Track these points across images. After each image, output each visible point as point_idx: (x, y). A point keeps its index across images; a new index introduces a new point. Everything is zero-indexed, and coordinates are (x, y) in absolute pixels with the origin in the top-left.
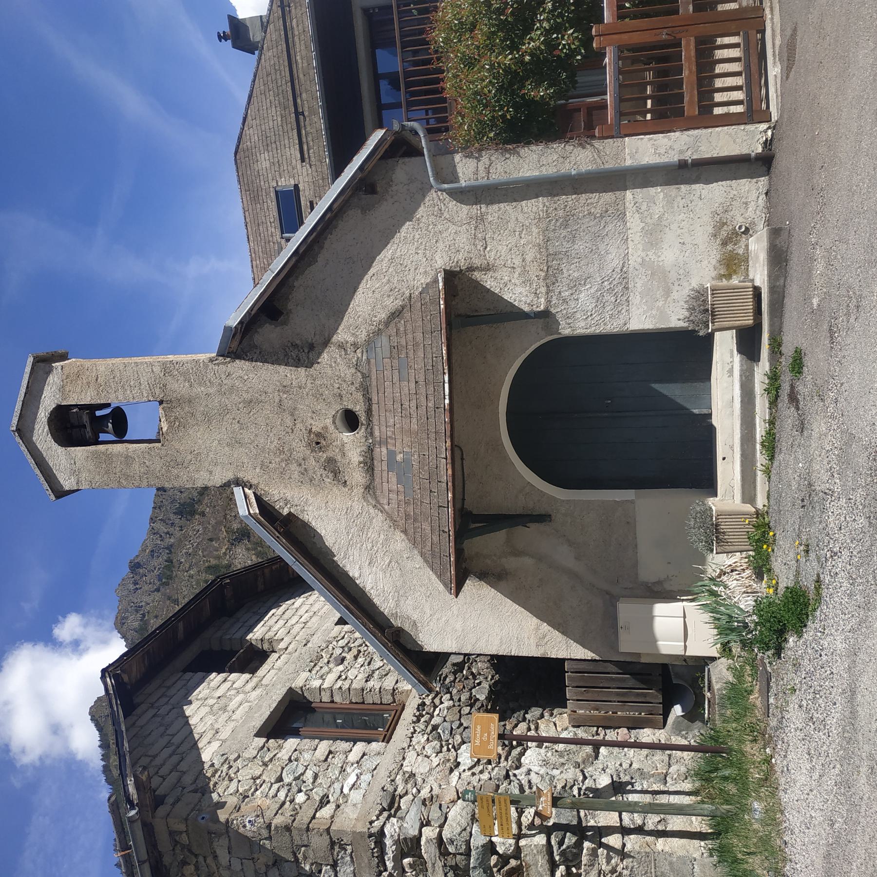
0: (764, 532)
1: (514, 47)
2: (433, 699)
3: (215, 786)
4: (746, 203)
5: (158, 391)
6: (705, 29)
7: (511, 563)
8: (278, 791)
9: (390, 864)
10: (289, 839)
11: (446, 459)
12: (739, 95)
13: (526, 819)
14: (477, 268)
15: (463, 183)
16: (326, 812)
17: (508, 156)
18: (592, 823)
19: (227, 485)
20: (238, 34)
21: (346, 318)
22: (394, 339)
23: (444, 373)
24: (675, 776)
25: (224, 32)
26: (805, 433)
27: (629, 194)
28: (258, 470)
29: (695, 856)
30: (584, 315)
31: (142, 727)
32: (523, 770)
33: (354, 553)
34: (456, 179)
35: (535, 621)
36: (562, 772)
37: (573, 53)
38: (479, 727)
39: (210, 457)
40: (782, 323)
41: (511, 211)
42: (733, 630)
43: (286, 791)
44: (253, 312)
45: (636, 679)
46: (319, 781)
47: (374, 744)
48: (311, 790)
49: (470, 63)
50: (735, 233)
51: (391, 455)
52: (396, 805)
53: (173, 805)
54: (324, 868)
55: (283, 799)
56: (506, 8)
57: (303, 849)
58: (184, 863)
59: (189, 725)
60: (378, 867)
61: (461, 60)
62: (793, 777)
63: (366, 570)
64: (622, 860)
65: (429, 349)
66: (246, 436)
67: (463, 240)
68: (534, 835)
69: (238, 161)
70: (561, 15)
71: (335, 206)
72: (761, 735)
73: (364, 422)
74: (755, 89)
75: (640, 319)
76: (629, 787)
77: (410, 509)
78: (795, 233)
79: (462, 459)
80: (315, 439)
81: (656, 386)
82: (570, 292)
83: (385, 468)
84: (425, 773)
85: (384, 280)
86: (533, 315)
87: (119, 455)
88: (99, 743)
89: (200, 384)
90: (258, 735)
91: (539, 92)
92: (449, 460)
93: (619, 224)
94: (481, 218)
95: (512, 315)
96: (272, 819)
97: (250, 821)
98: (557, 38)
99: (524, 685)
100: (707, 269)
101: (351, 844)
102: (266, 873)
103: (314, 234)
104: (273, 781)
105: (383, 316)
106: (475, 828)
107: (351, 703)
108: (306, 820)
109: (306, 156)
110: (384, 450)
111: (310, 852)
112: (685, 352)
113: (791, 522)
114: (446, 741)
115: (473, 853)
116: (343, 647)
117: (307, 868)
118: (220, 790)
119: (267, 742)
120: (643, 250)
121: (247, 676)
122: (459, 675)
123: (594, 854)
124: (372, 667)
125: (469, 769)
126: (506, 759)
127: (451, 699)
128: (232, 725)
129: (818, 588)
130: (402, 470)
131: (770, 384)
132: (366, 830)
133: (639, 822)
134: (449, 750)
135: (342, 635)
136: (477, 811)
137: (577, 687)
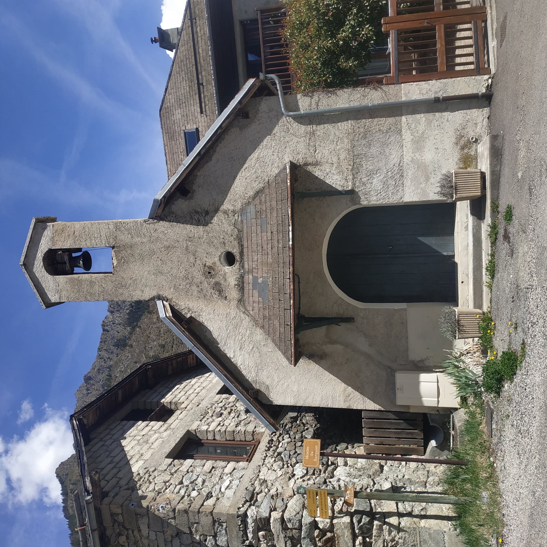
0: (488, 323)
1: (333, 36)
2: (278, 437)
3: (140, 486)
4: (476, 124)
5: (111, 240)
6: (450, 20)
7: (329, 348)
8: (180, 489)
9: (250, 536)
10: (186, 519)
11: (290, 279)
12: (471, 59)
13: (337, 508)
14: (310, 164)
15: (302, 112)
16: (210, 502)
17: (330, 95)
18: (379, 510)
19: (153, 299)
20: (164, 39)
21: (229, 195)
22: (258, 207)
23: (289, 225)
24: (432, 483)
25: (155, 38)
26: (514, 256)
27: (404, 118)
28: (172, 290)
29: (445, 530)
30: (376, 193)
31: (94, 452)
32: (335, 479)
33: (231, 342)
34: (298, 109)
35: (343, 385)
36: (360, 480)
37: (369, 39)
38: (308, 448)
39: (143, 282)
40: (499, 193)
41: (331, 129)
42: (469, 385)
43: (185, 490)
44: (172, 191)
45: (407, 423)
46: (206, 484)
47: (241, 463)
48: (201, 489)
49: (306, 47)
50: (469, 142)
51: (255, 279)
52: (255, 499)
53: (114, 497)
54: (208, 538)
55: (183, 494)
56: (328, 12)
57: (195, 525)
58: (120, 534)
59: (124, 451)
60: (243, 537)
61: (300, 46)
62: (508, 471)
63: (238, 353)
64: (398, 533)
65: (280, 211)
66: (166, 269)
67: (301, 147)
68: (342, 517)
69: (162, 115)
70: (361, 16)
71: (224, 125)
72: (487, 450)
73: (239, 260)
74: (481, 55)
75: (411, 195)
76: (403, 490)
77: (266, 313)
78: (506, 138)
79: (299, 283)
80: (208, 270)
81: (421, 238)
82: (367, 178)
83: (251, 287)
84: (274, 480)
85: (253, 172)
86: (344, 192)
87: (86, 280)
88: (61, 492)
89: (138, 236)
90: (168, 457)
91: (348, 63)
92: (291, 280)
93: (397, 136)
94: (313, 133)
95: (331, 192)
96: (176, 506)
97: (162, 507)
98: (359, 30)
99: (336, 428)
100: (452, 164)
101: (226, 522)
102: (171, 541)
103: (211, 142)
104: (177, 484)
105: (251, 193)
106: (305, 512)
107: (226, 440)
108: (198, 507)
109: (204, 110)
110: (251, 276)
111: (200, 527)
112: (440, 216)
113: (505, 313)
114: (287, 461)
115: (304, 528)
116: (221, 407)
117: (198, 538)
118: (143, 489)
119: (173, 461)
120: (413, 153)
121: (161, 423)
122: (294, 424)
123: (380, 529)
124: (240, 419)
125: (301, 478)
126: (325, 472)
127: (290, 437)
128: (151, 451)
129: (523, 349)
130: (261, 288)
131: (491, 232)
132: (236, 513)
133: (409, 510)
134: (288, 467)
135: (221, 400)
136: (306, 502)
137: (370, 428)
